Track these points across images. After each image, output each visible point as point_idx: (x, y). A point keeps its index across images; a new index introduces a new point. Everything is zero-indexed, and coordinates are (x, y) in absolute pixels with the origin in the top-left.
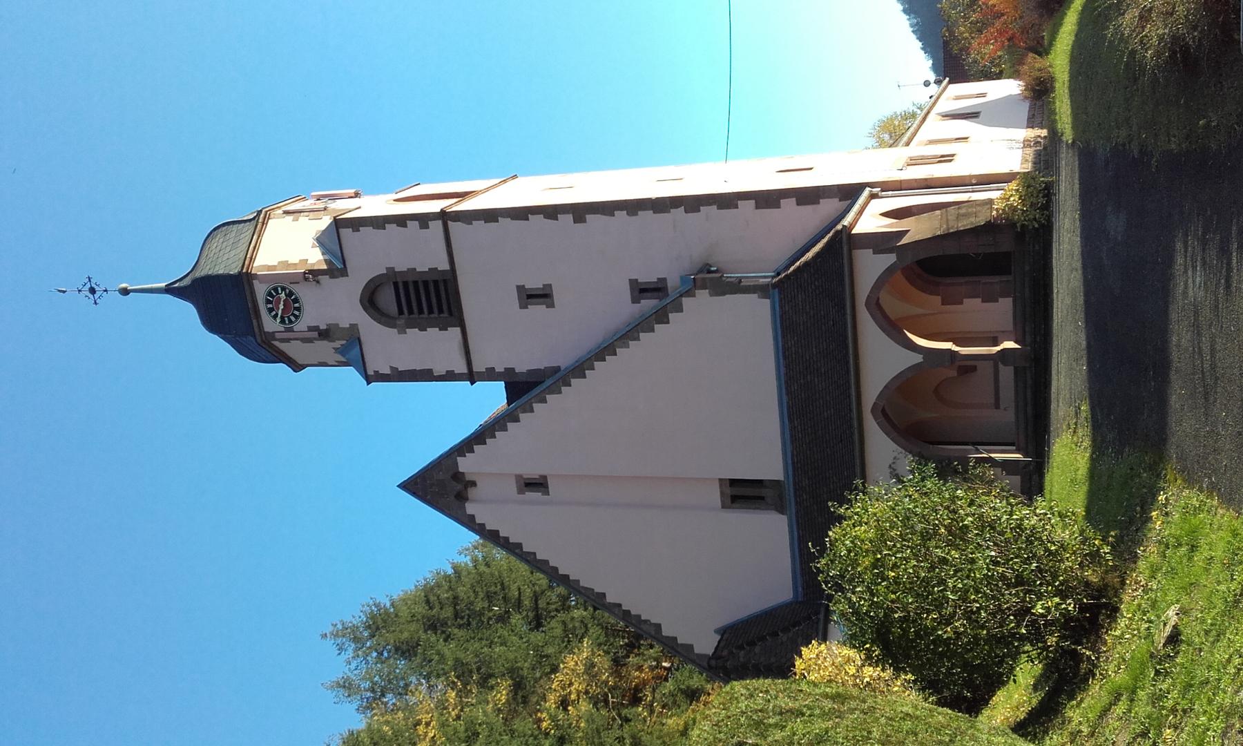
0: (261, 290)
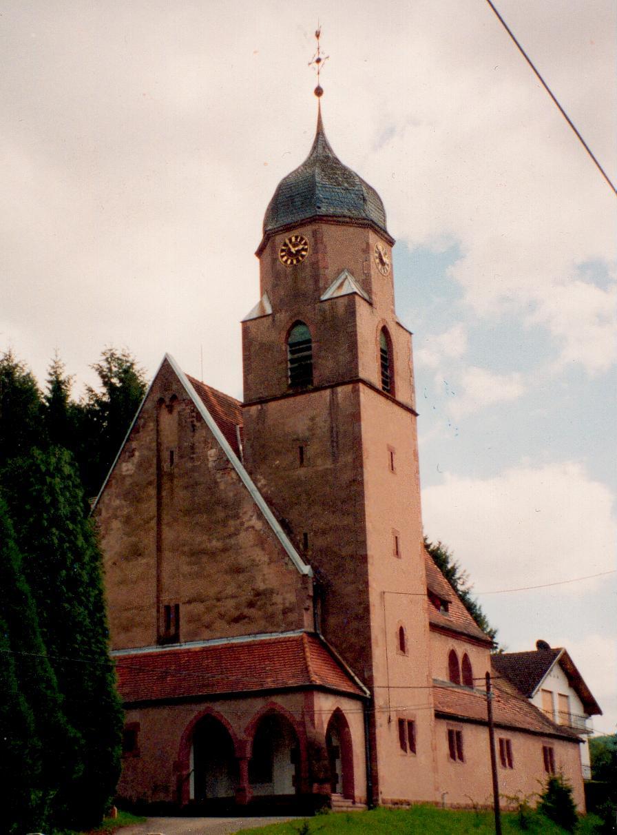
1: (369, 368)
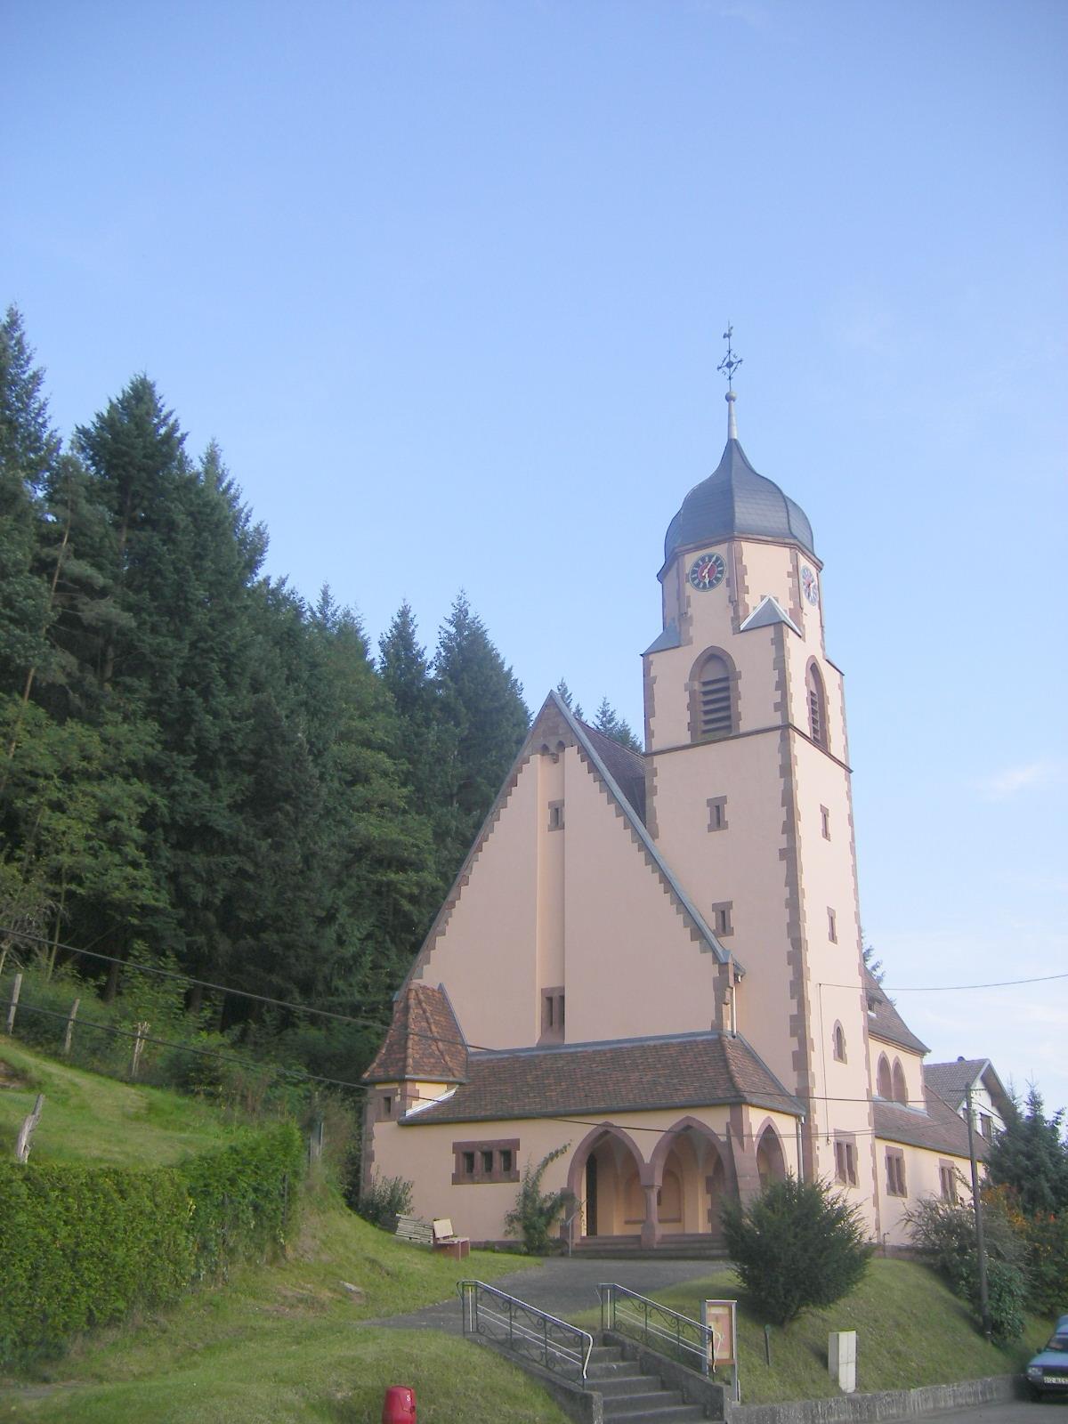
0: (720, 550)
1: (800, 715)
